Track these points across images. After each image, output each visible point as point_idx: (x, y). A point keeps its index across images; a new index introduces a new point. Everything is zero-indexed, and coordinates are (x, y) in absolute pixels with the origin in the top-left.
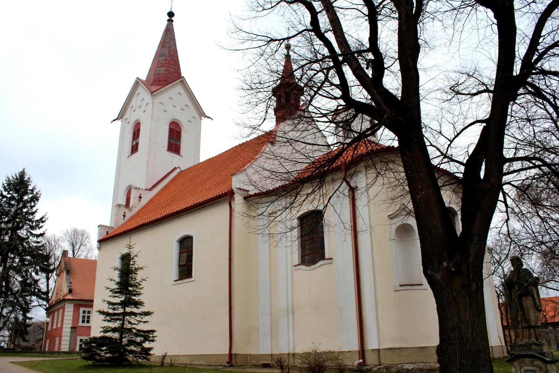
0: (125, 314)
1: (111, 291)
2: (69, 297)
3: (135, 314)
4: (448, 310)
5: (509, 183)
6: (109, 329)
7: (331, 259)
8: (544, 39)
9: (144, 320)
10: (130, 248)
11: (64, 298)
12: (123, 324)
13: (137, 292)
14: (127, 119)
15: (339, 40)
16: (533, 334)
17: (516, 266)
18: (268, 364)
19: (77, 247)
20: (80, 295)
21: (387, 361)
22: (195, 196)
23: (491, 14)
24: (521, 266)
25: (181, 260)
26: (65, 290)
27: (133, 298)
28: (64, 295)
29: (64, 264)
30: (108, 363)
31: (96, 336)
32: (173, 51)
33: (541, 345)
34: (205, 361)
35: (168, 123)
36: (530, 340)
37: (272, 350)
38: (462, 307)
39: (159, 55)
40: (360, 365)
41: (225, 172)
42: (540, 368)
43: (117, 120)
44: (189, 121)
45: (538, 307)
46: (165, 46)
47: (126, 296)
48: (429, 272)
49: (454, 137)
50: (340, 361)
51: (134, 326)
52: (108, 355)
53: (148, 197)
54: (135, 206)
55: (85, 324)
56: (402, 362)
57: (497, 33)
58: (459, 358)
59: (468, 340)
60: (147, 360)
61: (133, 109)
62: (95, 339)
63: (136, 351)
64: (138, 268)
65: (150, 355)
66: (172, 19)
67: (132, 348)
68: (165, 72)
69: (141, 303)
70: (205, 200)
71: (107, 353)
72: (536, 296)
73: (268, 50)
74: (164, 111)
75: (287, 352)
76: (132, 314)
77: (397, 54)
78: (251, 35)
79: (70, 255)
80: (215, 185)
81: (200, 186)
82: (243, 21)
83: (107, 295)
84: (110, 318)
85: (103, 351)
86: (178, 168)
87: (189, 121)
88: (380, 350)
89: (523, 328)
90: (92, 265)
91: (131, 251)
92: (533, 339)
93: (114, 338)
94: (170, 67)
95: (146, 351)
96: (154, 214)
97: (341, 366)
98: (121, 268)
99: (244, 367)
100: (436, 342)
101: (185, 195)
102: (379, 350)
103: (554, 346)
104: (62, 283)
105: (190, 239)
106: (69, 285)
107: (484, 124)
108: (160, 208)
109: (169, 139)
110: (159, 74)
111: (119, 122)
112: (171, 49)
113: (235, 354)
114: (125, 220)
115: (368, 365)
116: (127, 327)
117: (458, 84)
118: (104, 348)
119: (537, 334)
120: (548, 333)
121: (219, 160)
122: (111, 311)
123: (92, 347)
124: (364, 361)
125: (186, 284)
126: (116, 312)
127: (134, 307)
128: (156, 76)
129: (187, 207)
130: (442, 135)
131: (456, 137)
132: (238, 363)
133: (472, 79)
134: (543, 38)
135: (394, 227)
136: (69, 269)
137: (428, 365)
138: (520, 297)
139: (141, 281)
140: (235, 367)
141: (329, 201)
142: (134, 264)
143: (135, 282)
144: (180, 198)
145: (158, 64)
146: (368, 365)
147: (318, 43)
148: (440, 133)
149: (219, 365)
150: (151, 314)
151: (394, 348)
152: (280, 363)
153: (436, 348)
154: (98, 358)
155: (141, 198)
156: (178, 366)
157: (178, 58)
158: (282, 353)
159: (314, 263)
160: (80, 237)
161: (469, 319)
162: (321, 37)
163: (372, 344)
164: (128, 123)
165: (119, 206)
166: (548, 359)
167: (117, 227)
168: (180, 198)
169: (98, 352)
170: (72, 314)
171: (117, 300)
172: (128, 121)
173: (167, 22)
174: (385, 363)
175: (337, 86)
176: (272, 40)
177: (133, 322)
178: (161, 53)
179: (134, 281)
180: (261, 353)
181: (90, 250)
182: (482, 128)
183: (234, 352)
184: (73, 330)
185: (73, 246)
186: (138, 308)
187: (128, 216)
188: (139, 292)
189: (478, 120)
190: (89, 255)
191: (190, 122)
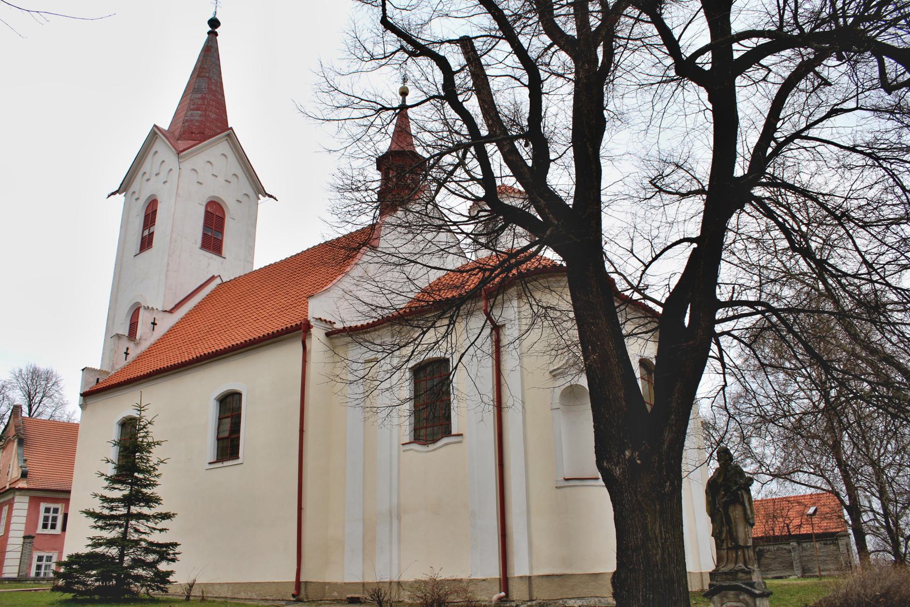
0: (129, 516)
1: (107, 479)
2: (22, 484)
3: (147, 518)
4: (629, 521)
5: (728, 333)
6: (102, 541)
7: (461, 435)
8: (783, 124)
9: (159, 526)
10: (140, 411)
11: (12, 486)
12: (125, 534)
13: (148, 480)
14: (134, 192)
15: (484, 106)
16: (741, 558)
17: (723, 462)
18: (358, 598)
19: (37, 399)
20: (42, 479)
21: (541, 594)
22: (247, 326)
23: (704, 94)
24: (729, 462)
25: (221, 430)
26: (15, 473)
27: (144, 490)
28: (13, 481)
29: (13, 428)
30: (97, 597)
31: (80, 553)
32: (216, 85)
33: (749, 572)
34: (257, 593)
35: (204, 204)
36: (737, 566)
37: (363, 576)
38: (649, 516)
39: (192, 90)
40: (501, 601)
41: (295, 290)
42: (747, 604)
43: (118, 194)
44: (238, 201)
45: (749, 519)
46: (202, 75)
47: (132, 488)
48: (605, 463)
49: (650, 259)
50: (469, 594)
51: (143, 536)
52: (97, 584)
53: (166, 323)
54: (145, 337)
55: (49, 531)
56: (564, 596)
57: (712, 121)
58: (643, 591)
59: (657, 565)
60: (163, 591)
61: (146, 177)
62: (76, 559)
63: (146, 577)
64: (153, 442)
65: (169, 582)
66: (216, 30)
67: (140, 571)
68: (201, 119)
69: (157, 500)
70: (264, 335)
71: (96, 580)
72: (747, 504)
73: (378, 122)
74: (198, 182)
75: (388, 580)
76: (140, 516)
77: (571, 131)
78: (353, 98)
79: (25, 413)
80: (279, 311)
81: (255, 310)
82: (339, 76)
83: (101, 486)
84: (104, 523)
85: (90, 576)
86: (217, 277)
87: (238, 201)
88: (532, 578)
89: (728, 549)
90: (69, 431)
91: (142, 415)
92: (741, 564)
93: (109, 556)
94: (211, 111)
95: (163, 578)
96: (178, 352)
97: (472, 602)
98: (120, 441)
99: (320, 602)
100: (611, 566)
101: (229, 323)
102: (530, 577)
103: (797, 570)
104: (9, 460)
105: (236, 397)
106: (21, 464)
107: (695, 245)
108: (188, 343)
109: (204, 229)
110: (192, 121)
111: (121, 198)
112: (213, 80)
113: (306, 583)
114: (128, 360)
115: (513, 601)
116: (132, 538)
117: (662, 176)
118: (94, 572)
119: (747, 557)
120: (790, 552)
121: (287, 269)
122: (106, 512)
123: (72, 571)
124: (507, 595)
125: (229, 469)
126: (114, 513)
127: (144, 506)
128: (186, 124)
129: (233, 345)
130: (634, 256)
131: (654, 259)
132: (310, 597)
133: (681, 173)
134: (781, 122)
135: (558, 392)
136: (23, 437)
137: (603, 600)
138: (726, 506)
139: (157, 464)
140: (305, 602)
141: (460, 361)
142: (146, 437)
143: (148, 465)
144: (221, 329)
145: (190, 104)
146: (513, 601)
147: (451, 113)
148: (632, 252)
149: (279, 600)
150: (171, 517)
151: (553, 575)
152: (378, 597)
153: (610, 576)
154: (82, 588)
155: (156, 324)
156: (214, 601)
157: (223, 95)
158: (381, 581)
159: (434, 441)
160: (43, 383)
161: (659, 534)
162: (459, 108)
163: (520, 568)
164: (137, 199)
165: (119, 336)
166: (757, 592)
167: (113, 372)
168: (221, 329)
169: (82, 578)
170: (25, 513)
171: (117, 494)
172: (136, 196)
173: (207, 35)
174: (539, 597)
175: (479, 181)
176: (384, 108)
177: (142, 530)
178: (196, 87)
179: (146, 463)
180: (347, 581)
181: (60, 404)
182: (688, 253)
183: (302, 579)
184: (28, 541)
185: (29, 397)
186: (150, 507)
187: (134, 353)
188: (154, 481)
189: (686, 237)
190: (58, 413)
191: (240, 202)
